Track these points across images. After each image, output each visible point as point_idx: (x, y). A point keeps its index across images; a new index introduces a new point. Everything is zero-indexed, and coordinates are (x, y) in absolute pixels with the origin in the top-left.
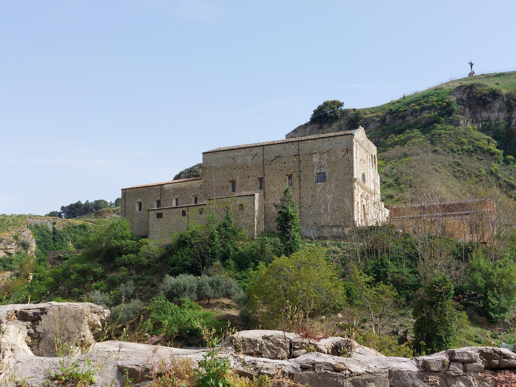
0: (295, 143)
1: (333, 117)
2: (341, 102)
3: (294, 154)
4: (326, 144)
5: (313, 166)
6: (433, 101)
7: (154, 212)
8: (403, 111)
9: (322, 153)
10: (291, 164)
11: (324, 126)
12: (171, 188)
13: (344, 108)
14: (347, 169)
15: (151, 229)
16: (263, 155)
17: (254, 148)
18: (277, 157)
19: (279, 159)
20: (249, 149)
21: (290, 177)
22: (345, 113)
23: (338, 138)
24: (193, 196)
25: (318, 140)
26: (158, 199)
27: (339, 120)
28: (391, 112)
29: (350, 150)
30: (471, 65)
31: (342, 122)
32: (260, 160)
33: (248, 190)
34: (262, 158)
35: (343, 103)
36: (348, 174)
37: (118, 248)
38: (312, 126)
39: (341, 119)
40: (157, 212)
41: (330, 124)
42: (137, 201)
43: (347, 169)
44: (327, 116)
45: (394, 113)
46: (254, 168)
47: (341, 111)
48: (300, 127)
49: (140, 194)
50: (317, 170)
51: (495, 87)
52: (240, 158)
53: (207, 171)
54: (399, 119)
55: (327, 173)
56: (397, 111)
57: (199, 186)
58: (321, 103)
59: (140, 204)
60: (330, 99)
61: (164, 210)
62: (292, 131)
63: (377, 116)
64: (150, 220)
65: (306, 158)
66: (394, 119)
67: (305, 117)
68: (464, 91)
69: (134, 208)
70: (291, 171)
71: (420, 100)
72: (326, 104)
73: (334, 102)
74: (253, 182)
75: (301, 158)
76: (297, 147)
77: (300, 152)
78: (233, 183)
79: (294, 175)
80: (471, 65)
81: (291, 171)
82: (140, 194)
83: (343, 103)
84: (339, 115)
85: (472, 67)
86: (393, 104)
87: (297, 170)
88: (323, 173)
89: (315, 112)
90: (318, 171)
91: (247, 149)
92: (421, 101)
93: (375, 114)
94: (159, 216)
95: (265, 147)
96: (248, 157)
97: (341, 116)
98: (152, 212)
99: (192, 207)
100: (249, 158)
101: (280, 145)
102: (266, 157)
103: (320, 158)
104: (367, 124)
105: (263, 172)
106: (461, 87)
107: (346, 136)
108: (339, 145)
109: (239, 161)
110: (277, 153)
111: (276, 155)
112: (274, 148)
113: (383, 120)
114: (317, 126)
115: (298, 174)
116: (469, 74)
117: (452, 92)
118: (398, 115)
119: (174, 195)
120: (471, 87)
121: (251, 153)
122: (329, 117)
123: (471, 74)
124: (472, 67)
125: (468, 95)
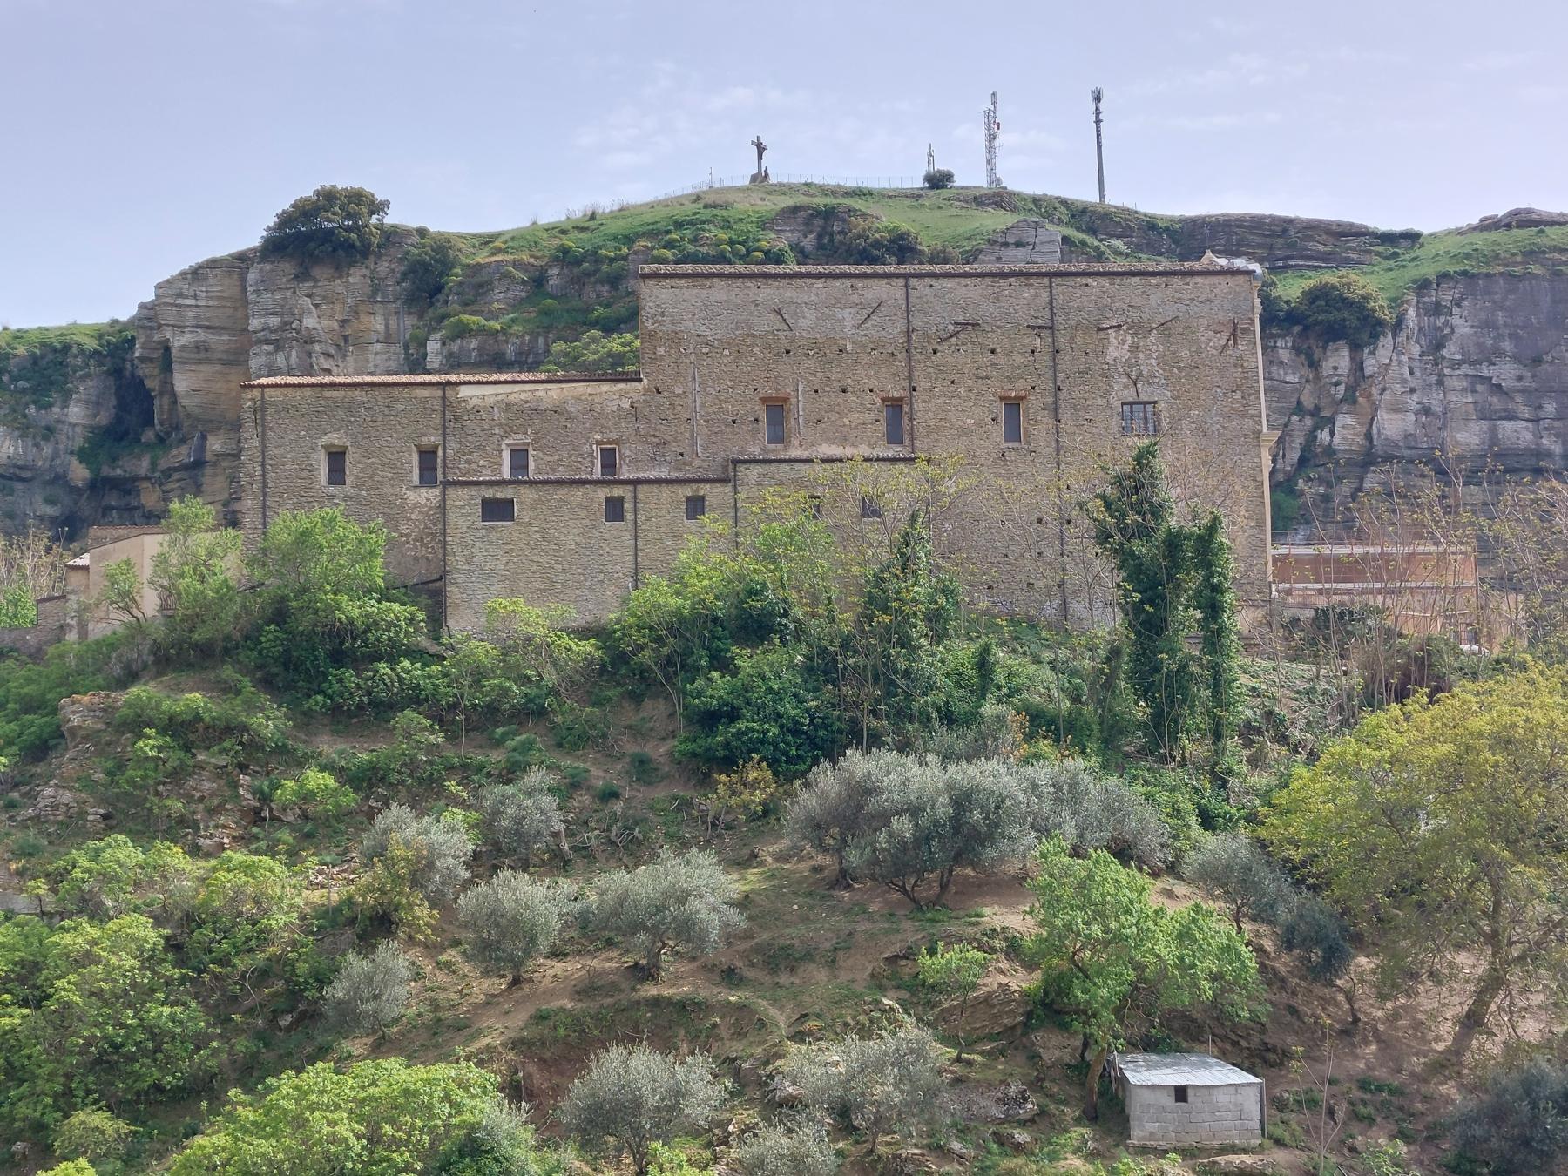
0: (1035, 281)
1: (352, 246)
2: (379, 197)
3: (1033, 322)
4: (1155, 298)
5: (1106, 375)
6: (720, 242)
7: (474, 491)
8: (611, 260)
9: (1140, 329)
10: (1019, 359)
11: (316, 271)
12: (491, 400)
13: (390, 220)
14: (1238, 396)
15: (457, 561)
16: (908, 311)
17: (869, 282)
18: (963, 326)
19: (970, 335)
20: (848, 282)
21: (1013, 406)
22: (393, 236)
23: (1199, 280)
24: (598, 443)
25: (1127, 280)
26: (430, 440)
27: (372, 258)
28: (564, 257)
29: (1245, 331)
30: (761, 149)
31: (383, 267)
32: (896, 329)
33: (844, 441)
34: (901, 325)
35: (387, 204)
36: (1243, 417)
37: (349, 630)
38: (268, 267)
39: (379, 256)
40: (489, 493)
41: (337, 268)
42: (325, 440)
43: (1238, 396)
44: (322, 237)
45: (578, 262)
46: (866, 359)
47: (380, 226)
48: (213, 264)
49: (340, 414)
50: (1121, 391)
51: (905, 227)
52: (810, 315)
53: (661, 351)
54: (602, 283)
55: (1162, 406)
56: (594, 256)
57: (626, 404)
58: (308, 192)
59: (337, 458)
60: (343, 182)
61: (522, 489)
62: (183, 274)
63: (515, 264)
64: (451, 522)
65: (1079, 340)
66: (580, 281)
67: (249, 232)
68: (806, 224)
69: (311, 469)
70: (1020, 384)
71: (668, 232)
72: (328, 197)
73: (357, 196)
74: (863, 412)
75: (1062, 340)
76: (1045, 296)
77: (1059, 319)
78: (777, 409)
79: (1034, 402)
80: (761, 149)
81: (1020, 384)
82: (340, 414)
83: (387, 204)
84: (375, 241)
85: (760, 157)
86: (563, 232)
87: (1047, 385)
88: (1145, 404)
89: (286, 220)
90: (1130, 395)
91: (838, 283)
92: (674, 236)
93: (509, 257)
94: (497, 510)
95: (913, 282)
96: (840, 314)
97: (379, 246)
98: (463, 492)
99: (654, 488)
100: (848, 317)
101: (977, 281)
102: (917, 323)
103: (1134, 348)
104: (481, 285)
105: (910, 378)
106: (795, 210)
107: (1229, 279)
108: (1206, 308)
109: (806, 322)
110: (964, 310)
111: (960, 319)
112: (951, 290)
113: (538, 281)
114: (288, 267)
115: (1050, 400)
116: (754, 178)
117: (772, 221)
118: (596, 271)
119: (507, 434)
120: (829, 214)
121: (856, 298)
122: (341, 245)
123: (760, 178)
124: (760, 157)
125: (820, 237)
